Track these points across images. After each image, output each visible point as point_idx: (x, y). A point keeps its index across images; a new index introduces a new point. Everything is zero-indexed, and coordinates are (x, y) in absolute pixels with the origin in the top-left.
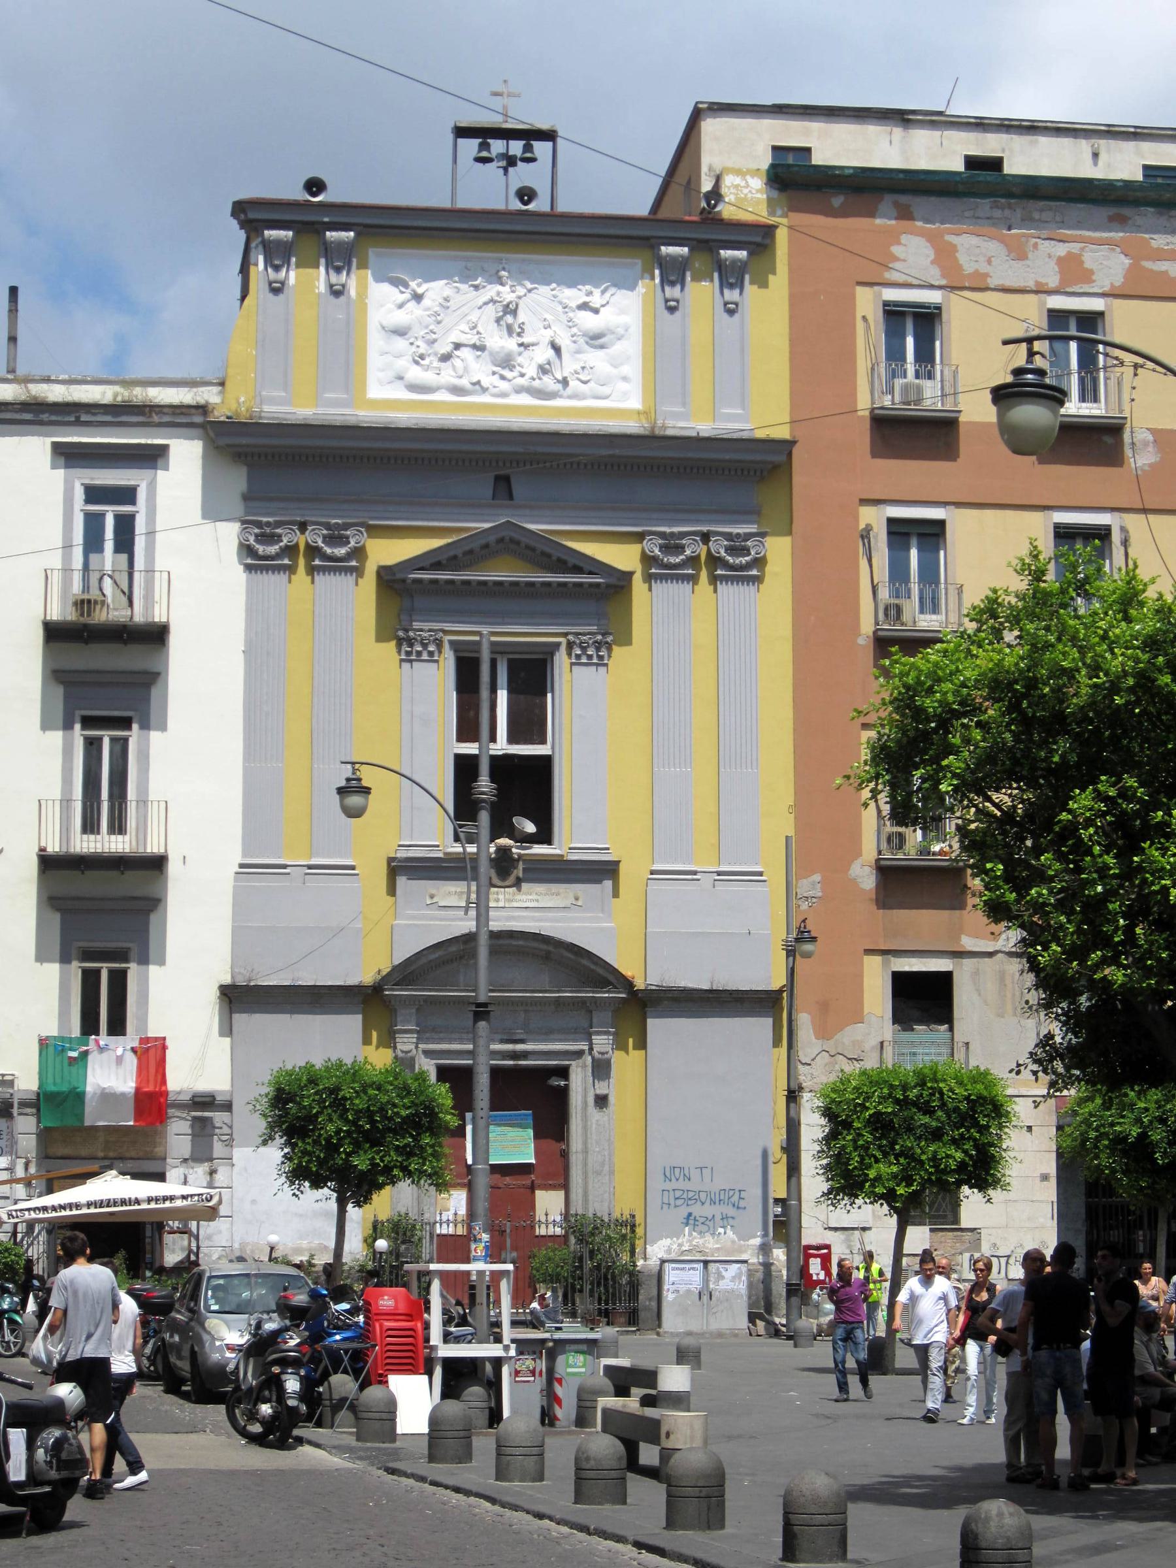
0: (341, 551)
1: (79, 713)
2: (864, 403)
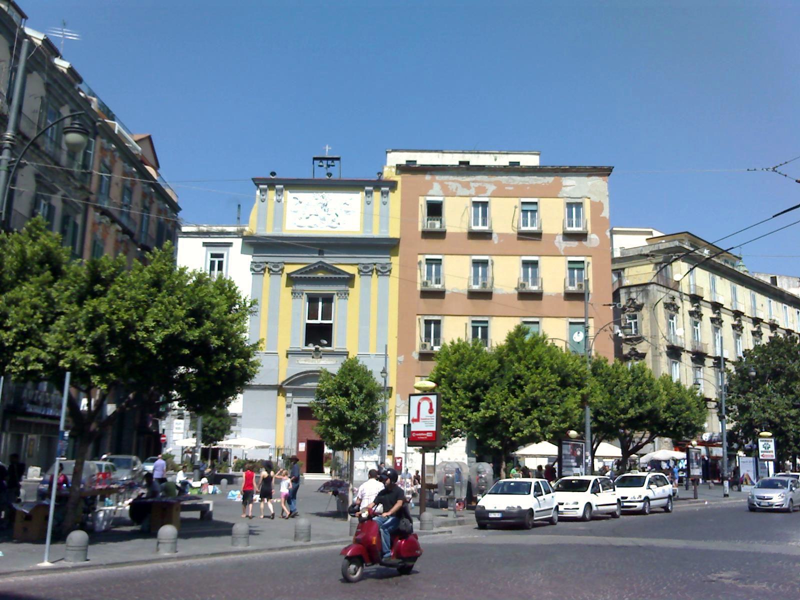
0: (277, 269)
2: (420, 229)
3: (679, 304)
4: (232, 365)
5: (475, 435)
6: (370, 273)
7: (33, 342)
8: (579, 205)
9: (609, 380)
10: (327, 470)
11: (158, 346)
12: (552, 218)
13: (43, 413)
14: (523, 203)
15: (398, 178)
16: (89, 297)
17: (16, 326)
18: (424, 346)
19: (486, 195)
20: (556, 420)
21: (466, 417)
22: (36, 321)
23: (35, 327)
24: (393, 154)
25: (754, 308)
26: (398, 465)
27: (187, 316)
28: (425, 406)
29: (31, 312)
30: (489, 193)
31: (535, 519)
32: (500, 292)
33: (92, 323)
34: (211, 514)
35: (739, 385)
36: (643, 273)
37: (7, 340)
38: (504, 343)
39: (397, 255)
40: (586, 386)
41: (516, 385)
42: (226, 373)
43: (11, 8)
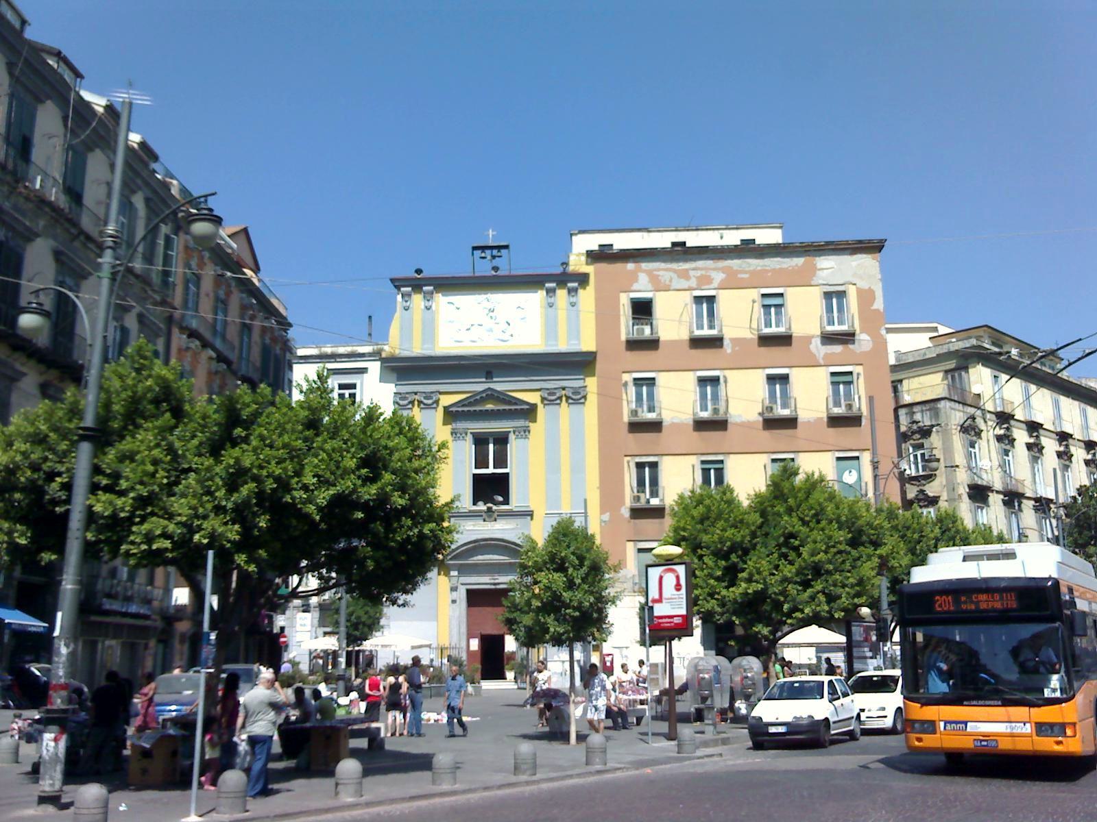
0: (430, 402)
2: (623, 337)
3: (982, 426)
4: (420, 532)
5: (734, 618)
6: (558, 401)
7: (156, 511)
8: (841, 295)
9: (909, 535)
10: (510, 675)
11: (320, 509)
12: (804, 313)
13: (124, 610)
14: (764, 296)
15: (589, 269)
16: (228, 445)
17: (133, 489)
18: (637, 499)
19: (712, 286)
20: (848, 593)
21: (718, 594)
22: (159, 480)
23: (156, 488)
24: (580, 236)
25: (1086, 427)
26: (608, 664)
27: (358, 468)
28: (669, 580)
29: (150, 468)
30: (715, 284)
31: (833, 732)
32: (738, 420)
33: (234, 481)
34: (382, 741)
35: (1076, 535)
36: (929, 385)
37: (122, 510)
38: (763, 489)
39: (594, 375)
40: (885, 544)
41: (789, 544)
42: (413, 544)
43: (61, 64)
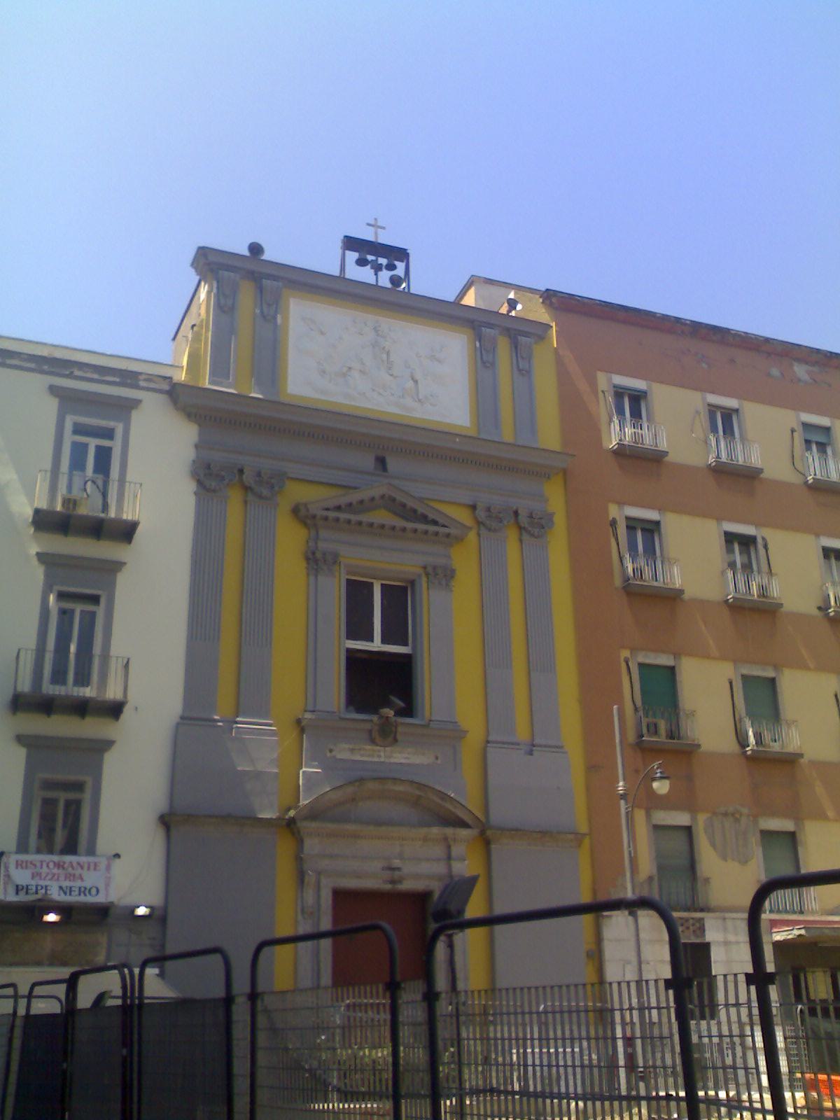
1: (57, 588)
